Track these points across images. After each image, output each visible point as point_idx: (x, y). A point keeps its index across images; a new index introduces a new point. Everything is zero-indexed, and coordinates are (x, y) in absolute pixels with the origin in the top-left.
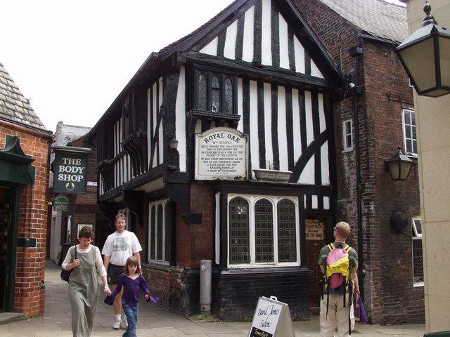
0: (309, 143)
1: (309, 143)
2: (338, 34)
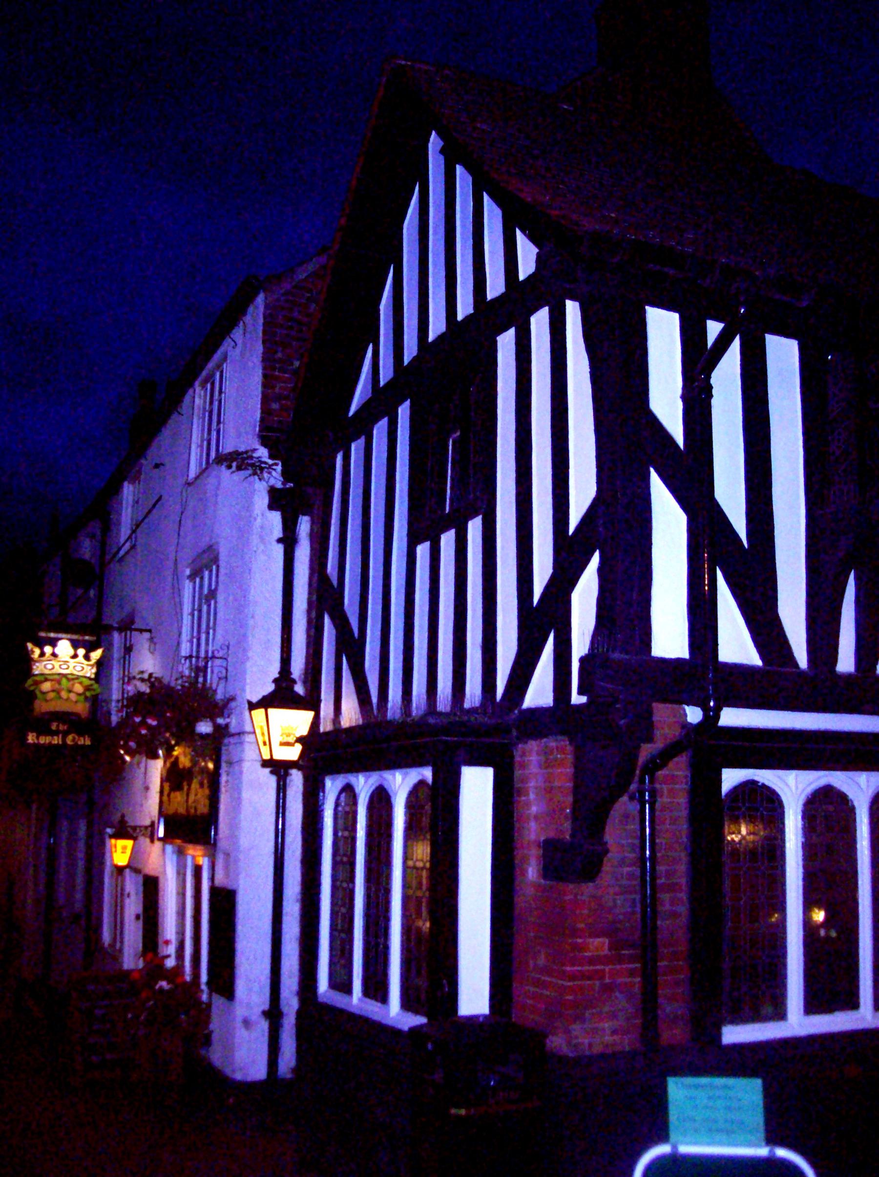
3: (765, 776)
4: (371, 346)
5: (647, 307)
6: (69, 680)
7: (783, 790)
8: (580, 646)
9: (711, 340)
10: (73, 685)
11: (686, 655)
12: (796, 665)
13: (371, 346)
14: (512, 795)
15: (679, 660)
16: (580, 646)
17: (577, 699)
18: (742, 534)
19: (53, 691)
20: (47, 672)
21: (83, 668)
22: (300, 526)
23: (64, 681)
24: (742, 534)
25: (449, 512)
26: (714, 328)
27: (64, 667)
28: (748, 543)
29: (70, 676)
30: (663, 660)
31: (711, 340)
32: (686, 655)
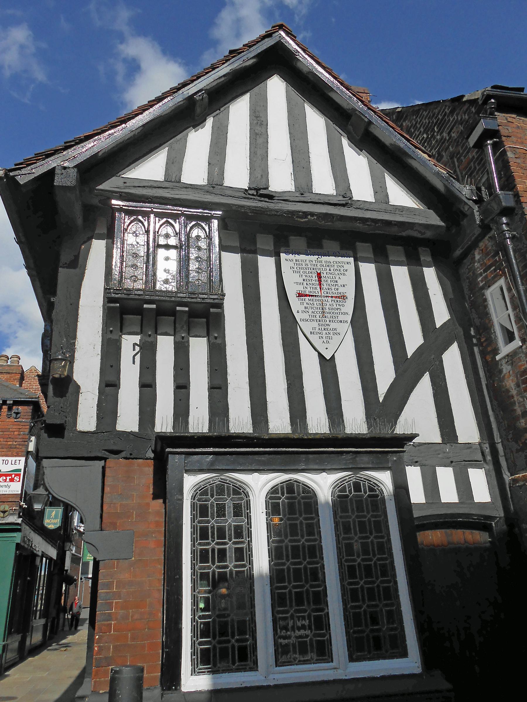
0: (410, 351)
1: (410, 351)
2: (445, 134)
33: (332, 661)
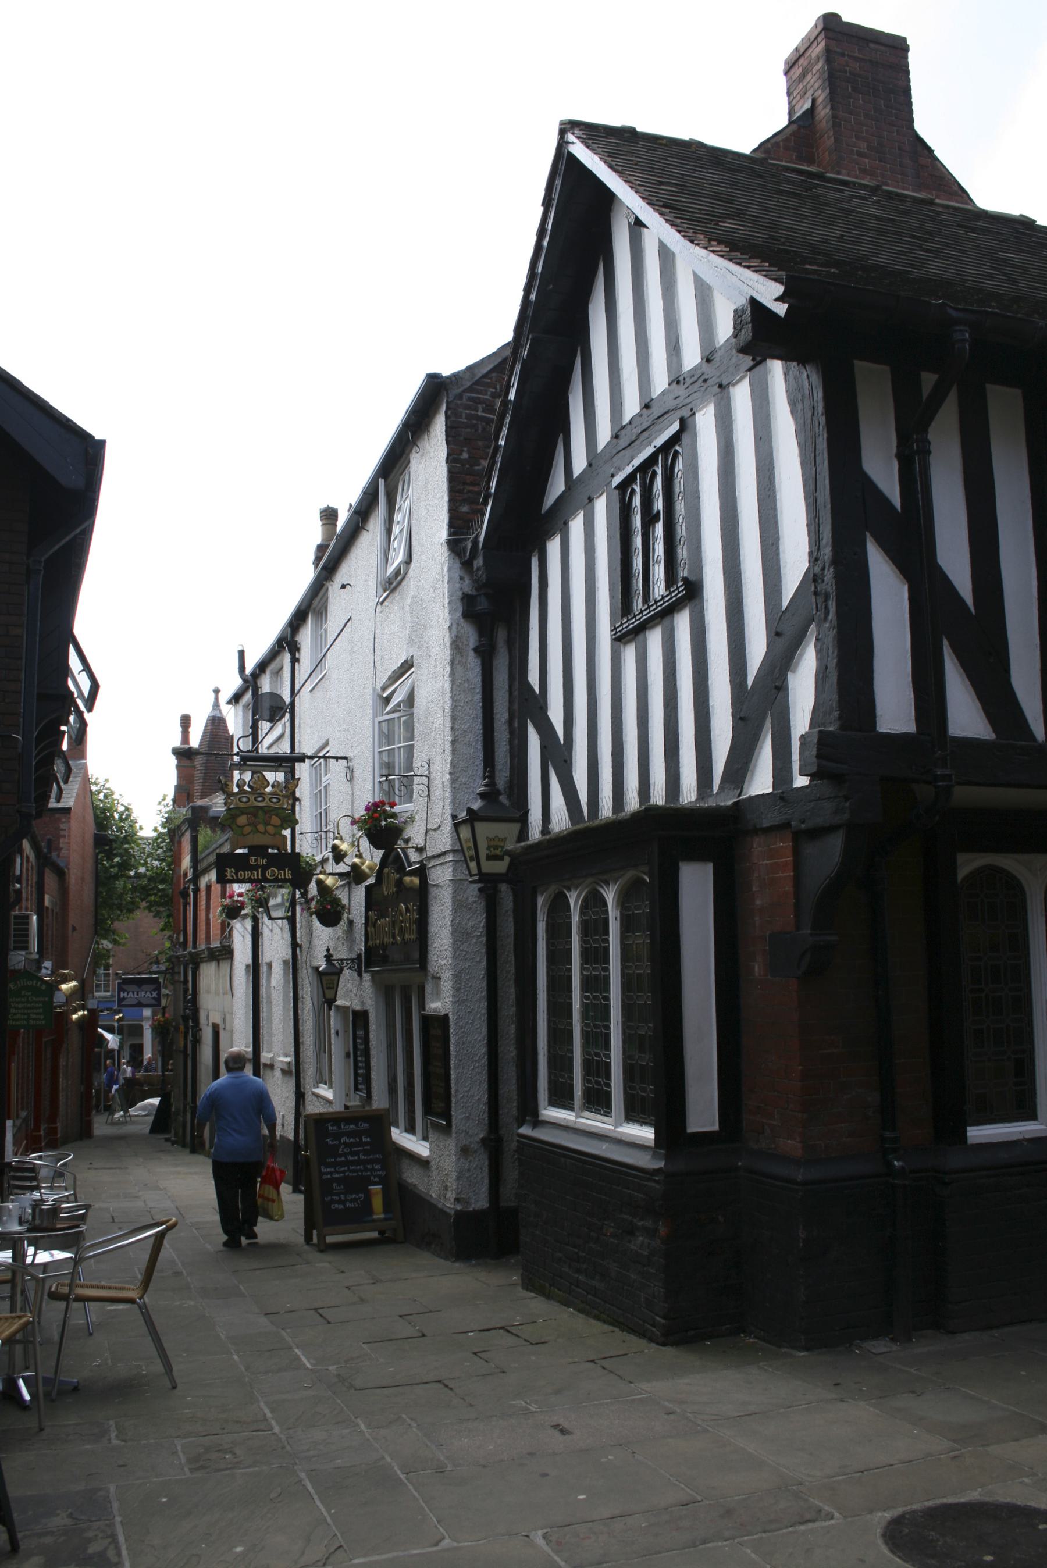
3: (1007, 862)
4: (561, 435)
5: (856, 362)
6: (266, 813)
7: (825, 503)
8: (801, 722)
9: (926, 391)
10: (270, 818)
11: (912, 728)
12: (1033, 738)
13: (561, 435)
14: (826, 412)
15: (905, 736)
16: (801, 722)
17: (801, 781)
18: (969, 599)
19: (249, 825)
20: (242, 805)
21: (279, 800)
22: (497, 633)
23: (260, 813)
24: (969, 599)
25: (97, 1031)
26: (929, 380)
27: (260, 799)
28: (975, 609)
29: (266, 808)
30: (887, 736)
31: (926, 391)
32: (912, 728)
33: (1032, 1116)
